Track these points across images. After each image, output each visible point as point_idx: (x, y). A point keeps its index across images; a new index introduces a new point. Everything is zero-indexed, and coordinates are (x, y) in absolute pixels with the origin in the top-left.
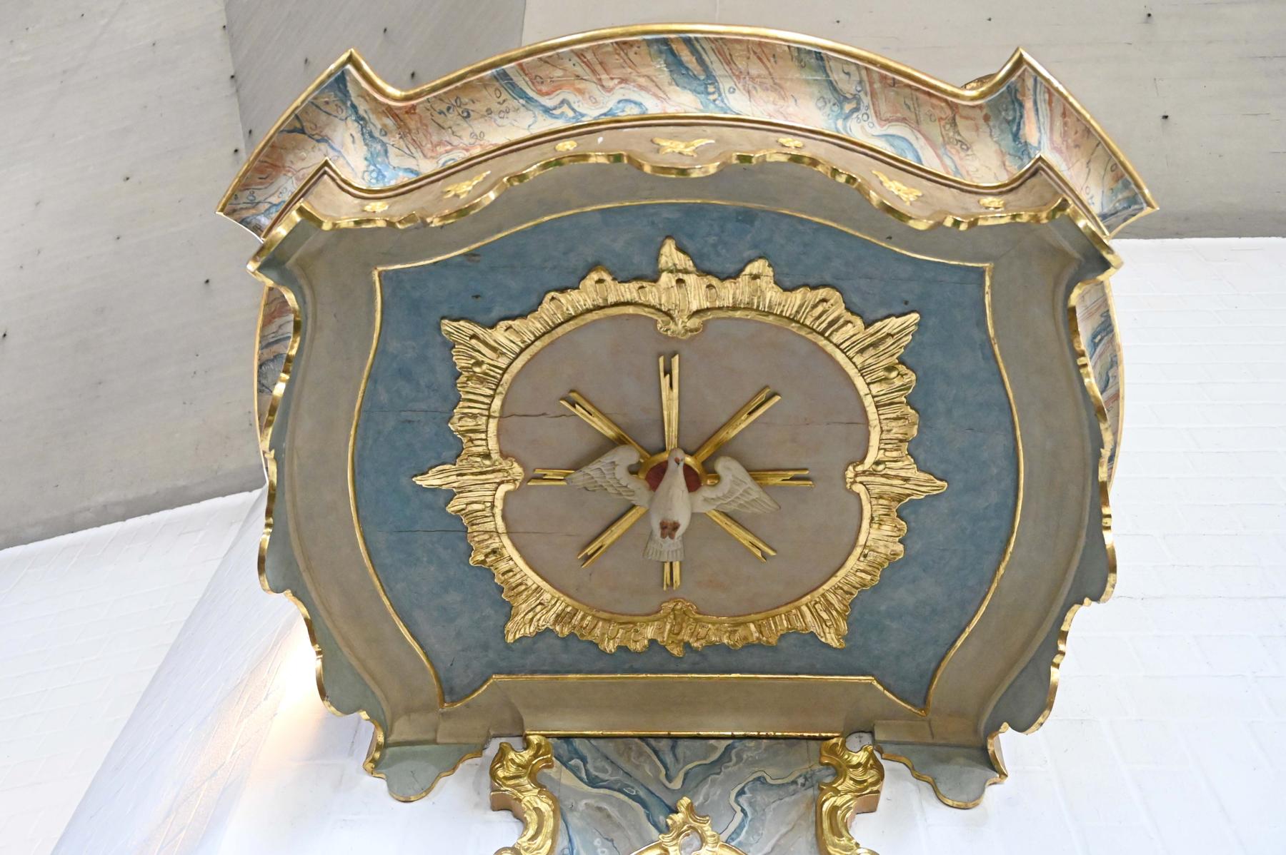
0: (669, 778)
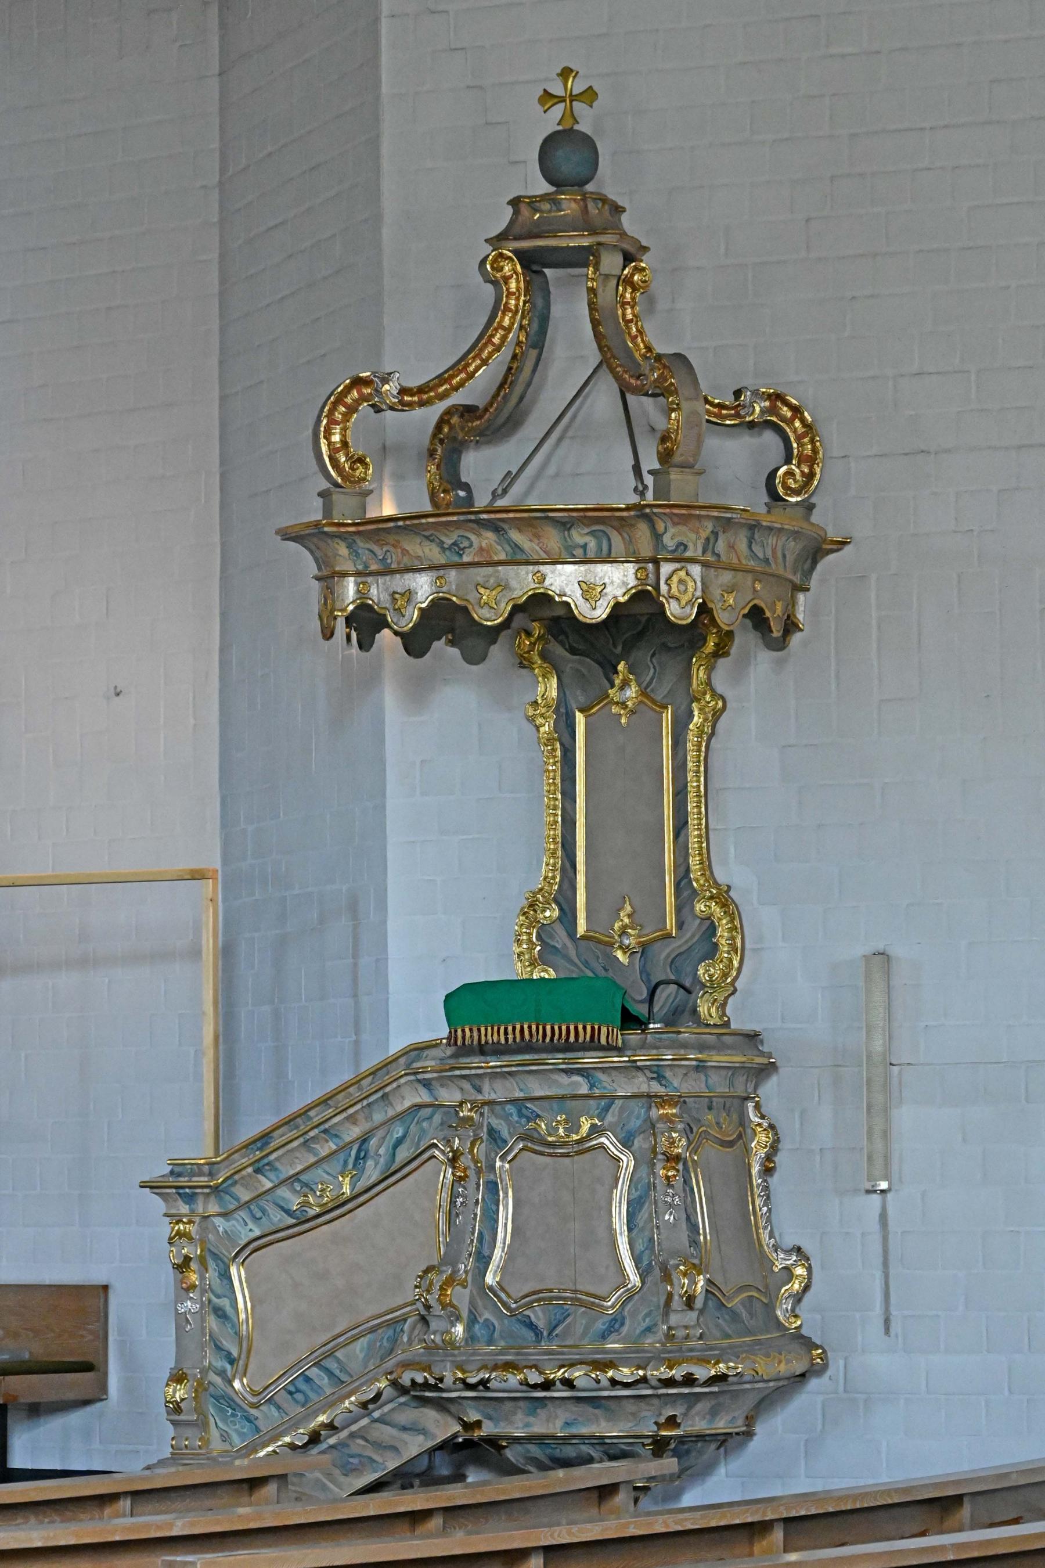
0: (615, 646)
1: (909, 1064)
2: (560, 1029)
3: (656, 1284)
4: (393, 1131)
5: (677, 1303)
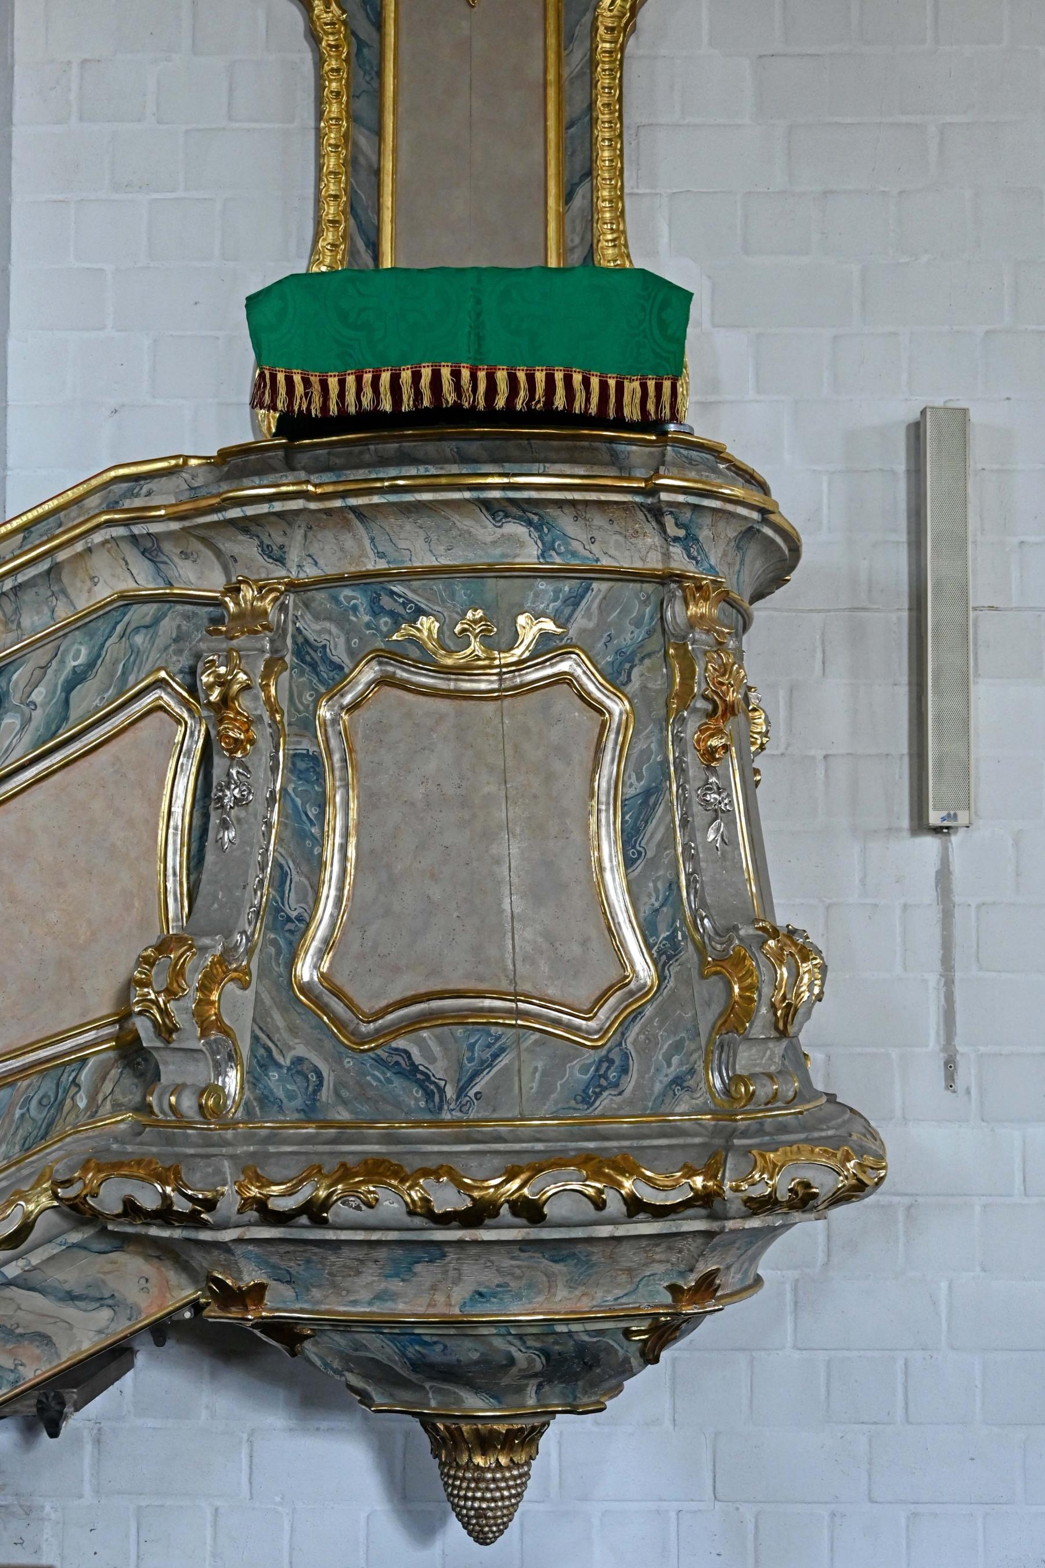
1: (991, 608)
2: (531, 379)
3: (688, 983)
4: (67, 651)
5: (759, 1026)
